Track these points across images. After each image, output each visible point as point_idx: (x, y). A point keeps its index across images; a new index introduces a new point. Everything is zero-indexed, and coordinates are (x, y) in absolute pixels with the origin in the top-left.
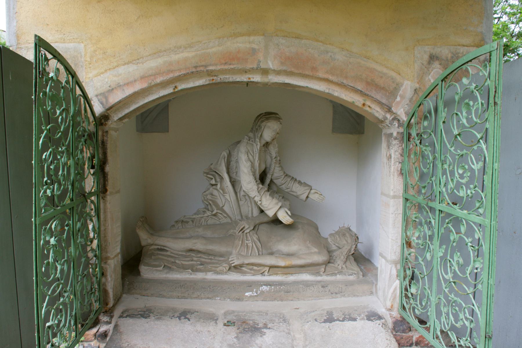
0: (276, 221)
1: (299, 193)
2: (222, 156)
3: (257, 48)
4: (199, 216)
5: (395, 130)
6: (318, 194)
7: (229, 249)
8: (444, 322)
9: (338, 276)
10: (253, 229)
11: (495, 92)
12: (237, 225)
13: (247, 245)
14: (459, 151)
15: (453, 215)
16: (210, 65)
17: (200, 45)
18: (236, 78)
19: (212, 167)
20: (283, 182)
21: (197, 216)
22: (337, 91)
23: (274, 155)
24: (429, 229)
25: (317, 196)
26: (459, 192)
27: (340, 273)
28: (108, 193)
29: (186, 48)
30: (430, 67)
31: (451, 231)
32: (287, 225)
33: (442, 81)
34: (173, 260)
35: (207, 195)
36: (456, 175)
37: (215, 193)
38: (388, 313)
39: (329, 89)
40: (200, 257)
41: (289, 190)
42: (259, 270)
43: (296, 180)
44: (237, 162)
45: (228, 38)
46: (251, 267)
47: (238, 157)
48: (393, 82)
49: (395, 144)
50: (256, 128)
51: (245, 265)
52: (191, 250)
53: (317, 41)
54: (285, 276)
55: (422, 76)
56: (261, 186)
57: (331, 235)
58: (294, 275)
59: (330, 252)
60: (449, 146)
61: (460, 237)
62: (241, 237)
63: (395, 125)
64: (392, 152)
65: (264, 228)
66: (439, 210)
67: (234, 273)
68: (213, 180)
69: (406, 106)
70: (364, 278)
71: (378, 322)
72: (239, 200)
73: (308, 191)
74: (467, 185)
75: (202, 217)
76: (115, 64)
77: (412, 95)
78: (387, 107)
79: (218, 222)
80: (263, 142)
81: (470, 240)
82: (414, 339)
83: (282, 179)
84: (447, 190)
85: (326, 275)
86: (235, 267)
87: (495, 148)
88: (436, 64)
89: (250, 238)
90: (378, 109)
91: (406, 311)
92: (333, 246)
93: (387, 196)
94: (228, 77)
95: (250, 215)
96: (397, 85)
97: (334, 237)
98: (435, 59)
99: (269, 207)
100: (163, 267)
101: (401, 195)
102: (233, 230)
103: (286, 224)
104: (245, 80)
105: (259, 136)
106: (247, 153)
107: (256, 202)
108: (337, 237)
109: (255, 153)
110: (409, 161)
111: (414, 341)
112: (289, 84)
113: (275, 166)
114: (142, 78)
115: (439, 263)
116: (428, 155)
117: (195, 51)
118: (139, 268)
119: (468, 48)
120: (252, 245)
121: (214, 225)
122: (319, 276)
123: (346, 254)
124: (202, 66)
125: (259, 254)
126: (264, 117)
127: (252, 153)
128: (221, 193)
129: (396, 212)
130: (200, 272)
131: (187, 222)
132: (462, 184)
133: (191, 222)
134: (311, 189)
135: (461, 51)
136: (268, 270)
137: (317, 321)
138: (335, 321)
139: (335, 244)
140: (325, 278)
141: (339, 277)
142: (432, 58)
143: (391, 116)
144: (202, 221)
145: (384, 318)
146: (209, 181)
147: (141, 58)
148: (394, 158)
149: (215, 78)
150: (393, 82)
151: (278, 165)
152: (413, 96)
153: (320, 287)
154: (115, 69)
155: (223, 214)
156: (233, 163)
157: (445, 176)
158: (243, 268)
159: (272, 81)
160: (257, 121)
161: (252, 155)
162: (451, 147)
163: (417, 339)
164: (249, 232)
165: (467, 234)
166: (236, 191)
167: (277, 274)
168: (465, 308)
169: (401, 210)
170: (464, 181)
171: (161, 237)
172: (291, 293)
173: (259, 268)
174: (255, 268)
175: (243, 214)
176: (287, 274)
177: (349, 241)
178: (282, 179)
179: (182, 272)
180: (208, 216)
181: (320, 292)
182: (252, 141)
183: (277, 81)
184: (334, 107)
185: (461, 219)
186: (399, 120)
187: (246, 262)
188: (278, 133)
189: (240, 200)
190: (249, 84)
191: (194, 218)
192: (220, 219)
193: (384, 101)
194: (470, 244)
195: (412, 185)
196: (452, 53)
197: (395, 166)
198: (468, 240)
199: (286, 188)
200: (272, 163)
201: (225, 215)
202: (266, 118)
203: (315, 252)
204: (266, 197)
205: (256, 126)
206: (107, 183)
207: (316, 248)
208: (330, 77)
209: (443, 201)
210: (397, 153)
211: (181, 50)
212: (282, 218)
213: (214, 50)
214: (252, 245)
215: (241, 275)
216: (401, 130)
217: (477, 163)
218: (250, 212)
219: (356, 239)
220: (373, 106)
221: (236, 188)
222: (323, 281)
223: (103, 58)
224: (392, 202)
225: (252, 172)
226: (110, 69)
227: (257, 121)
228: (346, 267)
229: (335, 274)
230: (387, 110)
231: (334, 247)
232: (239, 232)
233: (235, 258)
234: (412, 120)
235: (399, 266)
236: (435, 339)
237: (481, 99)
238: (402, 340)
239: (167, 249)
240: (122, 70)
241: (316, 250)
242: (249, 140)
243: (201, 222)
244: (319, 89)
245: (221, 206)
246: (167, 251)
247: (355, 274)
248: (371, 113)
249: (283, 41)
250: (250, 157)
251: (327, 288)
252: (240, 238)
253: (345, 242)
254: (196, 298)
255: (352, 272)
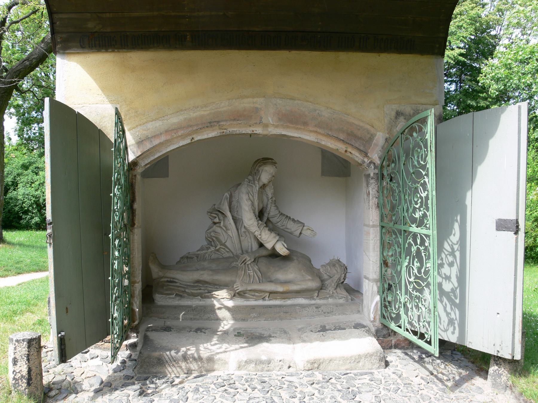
0: (274, 255)
1: (293, 230)
2: (224, 196)
3: (260, 107)
4: (204, 252)
5: (372, 172)
6: (310, 231)
7: (233, 279)
8: (410, 315)
9: (329, 299)
10: (254, 261)
11: (431, 143)
12: (239, 259)
13: (249, 274)
14: (413, 185)
15: (412, 232)
16: (222, 121)
17: (214, 105)
18: (243, 131)
19: (216, 207)
20: (278, 220)
21: (202, 252)
22: (324, 141)
23: (270, 196)
24: (398, 247)
25: (309, 232)
26: (415, 215)
27: (332, 296)
28: (136, 226)
29: (202, 108)
30: (397, 121)
31: (412, 245)
32: (284, 256)
33: (401, 134)
34: (183, 290)
35: (211, 233)
36: (413, 202)
37: (218, 230)
38: (371, 324)
39: (318, 139)
40: (207, 287)
41: (284, 227)
42: (261, 296)
43: (290, 218)
44: (238, 202)
45: (236, 100)
46: (253, 293)
47: (239, 197)
48: (368, 133)
49: (372, 183)
50: (255, 171)
51: (248, 292)
52: (198, 281)
53: (307, 101)
54: (284, 300)
55: (391, 128)
56: (260, 222)
57: (322, 266)
58: (292, 299)
59: (322, 281)
60: (407, 182)
61: (417, 247)
62: (244, 268)
63: (372, 167)
64: (370, 189)
65: (263, 263)
66: (404, 230)
67: (238, 299)
68: (217, 218)
69: (379, 152)
70: (352, 302)
71: (363, 329)
72: (240, 236)
73: (301, 228)
74: (419, 209)
75: (206, 253)
76: (145, 121)
77: (384, 143)
78: (364, 153)
79: (221, 257)
80: (261, 184)
81: (423, 248)
82: (393, 342)
83: (277, 217)
84: (408, 215)
85: (319, 299)
86: (238, 293)
87: (433, 181)
88: (402, 119)
89: (251, 269)
90: (357, 154)
91: (386, 319)
92: (325, 275)
93: (368, 226)
94: (235, 130)
95: (250, 250)
96: (372, 135)
97: (326, 267)
98: (400, 115)
99: (268, 241)
100: (175, 295)
101: (379, 224)
102: (236, 262)
103: (283, 255)
104: (250, 132)
105: (258, 179)
106: (248, 193)
107: (256, 236)
108: (328, 267)
109: (254, 193)
110: (383, 196)
111: (393, 345)
112: (285, 135)
113: (271, 206)
114: (167, 131)
115: (405, 271)
116: (395, 190)
117: (210, 110)
118: (153, 297)
119: (426, 106)
120: (254, 274)
121: (218, 259)
122: (313, 300)
123: (336, 282)
124: (215, 122)
125: (259, 282)
126: (261, 162)
127: (251, 193)
128: (224, 230)
129: (375, 239)
130: (208, 298)
131: (192, 258)
132: (417, 208)
133: (196, 258)
134: (304, 226)
135: (421, 108)
136: (268, 296)
137: (312, 332)
138: (327, 330)
139: (326, 274)
140: (318, 302)
141: (330, 300)
142: (398, 114)
143: (368, 160)
144: (206, 256)
145: (368, 327)
146: (212, 220)
147: (166, 116)
148: (372, 194)
149: (225, 131)
150: (368, 133)
151: (274, 205)
152: (384, 144)
153: (314, 308)
154: (145, 125)
155: (226, 249)
156: (234, 203)
157: (406, 204)
158: (247, 295)
159: (271, 133)
160: (255, 166)
161: (251, 195)
162: (409, 182)
163: (395, 342)
164: (250, 264)
165: (421, 245)
166: (238, 227)
167: (276, 299)
168: (422, 298)
169: (378, 238)
170: (417, 206)
171: (171, 270)
172: (289, 314)
173: (260, 294)
174: (257, 294)
175: (243, 249)
176: (285, 298)
177: (339, 271)
178: (277, 217)
179: (192, 299)
180: (211, 252)
181: (315, 312)
182: (252, 183)
183: (276, 133)
184: (322, 151)
185: (417, 234)
186: (374, 164)
187: (249, 288)
188: (273, 176)
189: (241, 236)
190: (252, 135)
191: (199, 254)
192: (223, 254)
193: (362, 148)
194: (423, 251)
195: (386, 214)
196: (414, 110)
197: (373, 201)
198: (422, 248)
199: (281, 226)
200: (269, 203)
201: (228, 250)
202: (263, 163)
203: (309, 280)
204: (265, 231)
205: (254, 170)
206: (135, 218)
207: (310, 276)
208: (318, 130)
209: (406, 223)
210: (374, 190)
211: (198, 109)
212: (280, 250)
213: (225, 109)
214: (254, 274)
215: (245, 300)
216: (376, 171)
217: (424, 192)
218: (250, 247)
219: (344, 269)
220: (353, 152)
221: (238, 225)
222: (317, 304)
223: (135, 116)
224: (372, 230)
225: (253, 210)
226: (140, 125)
227: (255, 166)
228: (336, 292)
229: (327, 298)
230: (364, 155)
231: (325, 277)
232: (241, 264)
233: (239, 285)
234: (384, 163)
235: (379, 284)
236: (406, 331)
237: (424, 148)
238: (383, 343)
239: (176, 281)
240: (150, 125)
241: (310, 278)
242: (249, 182)
243: (205, 257)
244: (309, 139)
245: (224, 242)
246: (176, 282)
247: (344, 298)
248: (352, 158)
249: (279, 101)
250: (251, 197)
251: (320, 308)
252: (242, 269)
253: (335, 272)
254: (207, 319)
255: (341, 296)
